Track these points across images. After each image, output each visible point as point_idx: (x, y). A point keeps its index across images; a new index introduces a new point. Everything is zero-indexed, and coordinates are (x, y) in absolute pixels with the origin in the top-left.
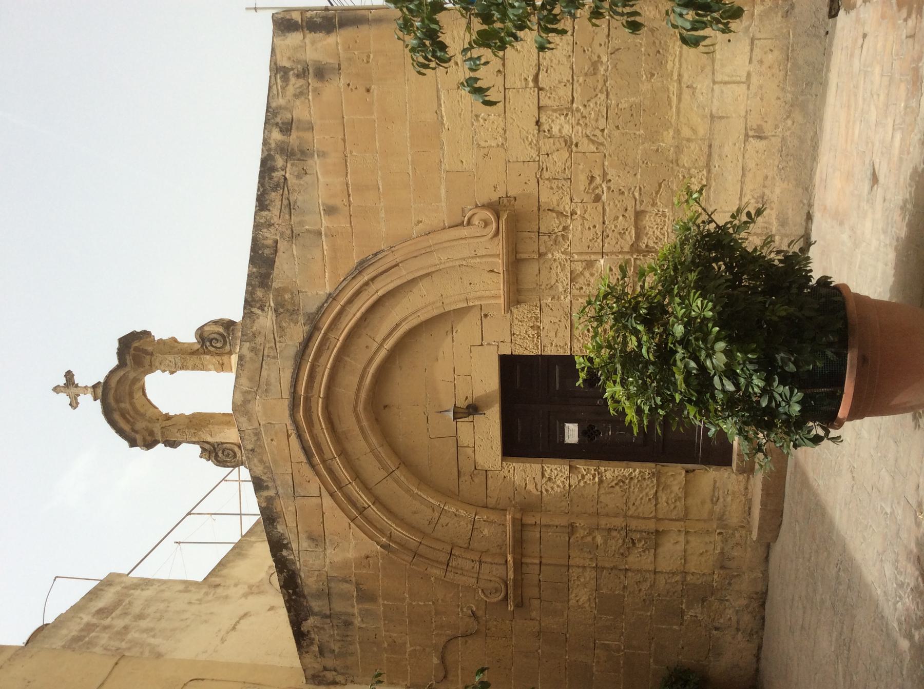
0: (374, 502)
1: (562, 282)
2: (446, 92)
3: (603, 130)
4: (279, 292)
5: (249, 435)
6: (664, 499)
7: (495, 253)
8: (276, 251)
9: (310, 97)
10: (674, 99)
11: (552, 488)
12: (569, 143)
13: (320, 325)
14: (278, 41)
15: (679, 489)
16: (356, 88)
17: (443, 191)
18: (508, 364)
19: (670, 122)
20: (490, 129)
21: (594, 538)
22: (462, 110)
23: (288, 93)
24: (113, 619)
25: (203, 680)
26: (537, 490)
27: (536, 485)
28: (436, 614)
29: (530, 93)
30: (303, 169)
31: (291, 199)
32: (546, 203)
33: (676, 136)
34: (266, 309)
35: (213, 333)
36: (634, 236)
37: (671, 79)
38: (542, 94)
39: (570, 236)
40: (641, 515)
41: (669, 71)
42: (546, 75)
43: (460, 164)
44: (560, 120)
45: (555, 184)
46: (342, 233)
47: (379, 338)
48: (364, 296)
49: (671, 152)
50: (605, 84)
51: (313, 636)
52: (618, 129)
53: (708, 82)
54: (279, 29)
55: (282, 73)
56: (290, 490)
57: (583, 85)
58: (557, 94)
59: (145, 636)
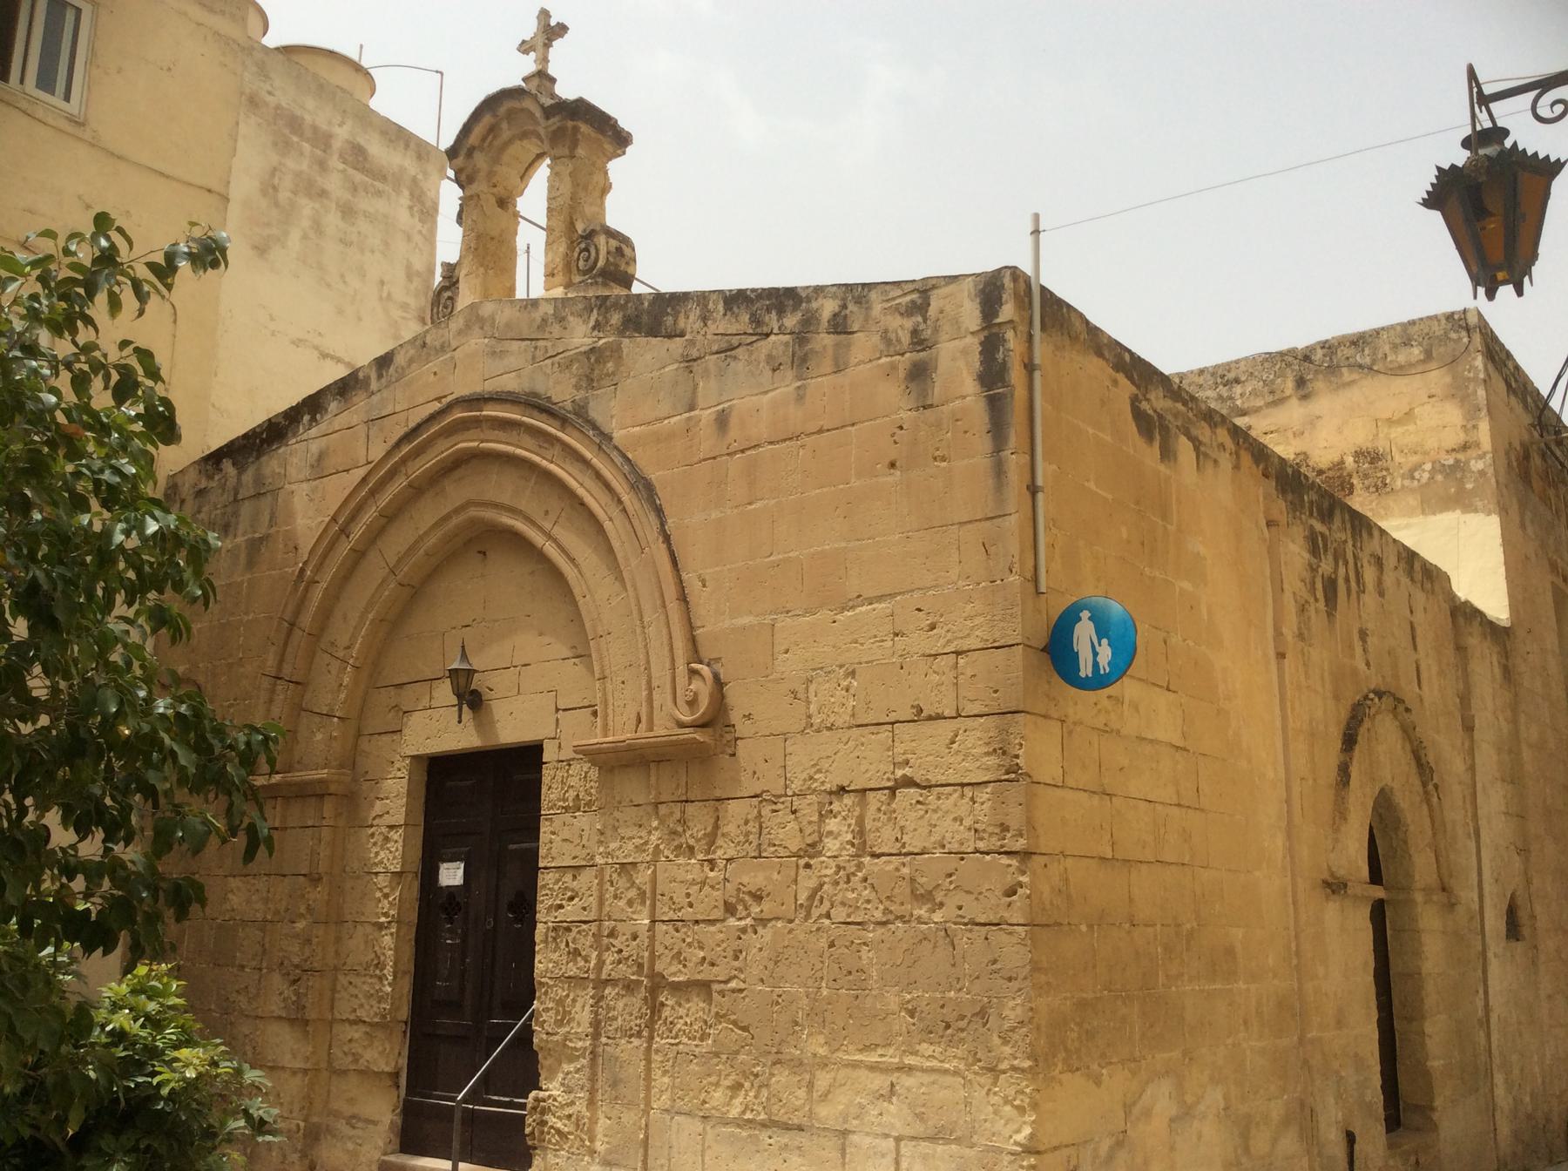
0: (355, 551)
1: (621, 847)
2: (889, 611)
3: (828, 916)
4: (616, 350)
5: (443, 336)
6: (356, 1036)
7: (656, 722)
8: (670, 337)
9: (884, 360)
10: (873, 1058)
11: (375, 844)
12: (813, 849)
13: (569, 429)
14: (968, 285)
15: (368, 1061)
16: (896, 443)
17: (746, 620)
18: (529, 756)
19: (838, 1050)
20: (833, 700)
21: (302, 916)
22: (862, 644)
23: (889, 318)
24: (343, 171)
25: (175, 322)
26: (374, 819)
27: (381, 816)
28: (230, 666)
29: (885, 774)
30: (780, 364)
31: (740, 350)
32: (727, 811)
33: (817, 1060)
34: (596, 333)
35: (596, 246)
36: (676, 979)
37: (904, 1051)
38: (883, 796)
39: (681, 860)
40: (337, 995)
41: (918, 1047)
42: (914, 802)
43: (783, 648)
44: (847, 832)
45: (753, 827)
46: (691, 447)
47: (558, 532)
48: (604, 497)
49: (793, 1050)
50: (897, 918)
51: (217, 478)
52: (830, 947)
53: (899, 1128)
54: (987, 284)
55: (919, 301)
56: (375, 415)
57: (897, 874)
58: (884, 825)
59: (306, 223)
